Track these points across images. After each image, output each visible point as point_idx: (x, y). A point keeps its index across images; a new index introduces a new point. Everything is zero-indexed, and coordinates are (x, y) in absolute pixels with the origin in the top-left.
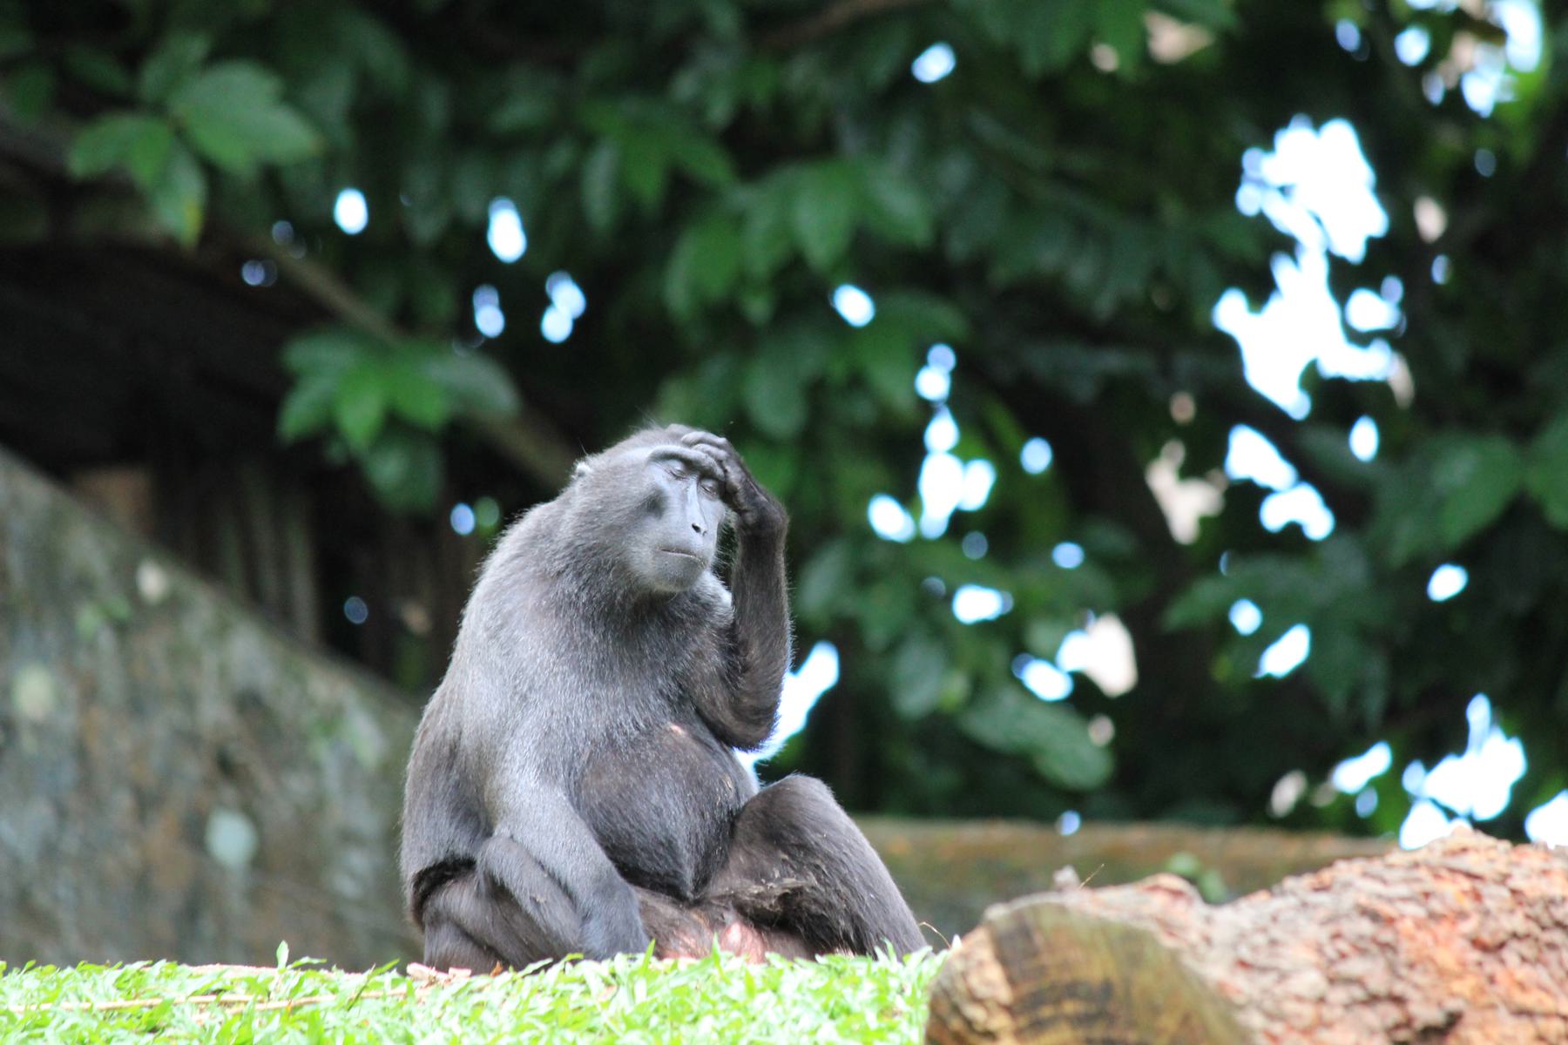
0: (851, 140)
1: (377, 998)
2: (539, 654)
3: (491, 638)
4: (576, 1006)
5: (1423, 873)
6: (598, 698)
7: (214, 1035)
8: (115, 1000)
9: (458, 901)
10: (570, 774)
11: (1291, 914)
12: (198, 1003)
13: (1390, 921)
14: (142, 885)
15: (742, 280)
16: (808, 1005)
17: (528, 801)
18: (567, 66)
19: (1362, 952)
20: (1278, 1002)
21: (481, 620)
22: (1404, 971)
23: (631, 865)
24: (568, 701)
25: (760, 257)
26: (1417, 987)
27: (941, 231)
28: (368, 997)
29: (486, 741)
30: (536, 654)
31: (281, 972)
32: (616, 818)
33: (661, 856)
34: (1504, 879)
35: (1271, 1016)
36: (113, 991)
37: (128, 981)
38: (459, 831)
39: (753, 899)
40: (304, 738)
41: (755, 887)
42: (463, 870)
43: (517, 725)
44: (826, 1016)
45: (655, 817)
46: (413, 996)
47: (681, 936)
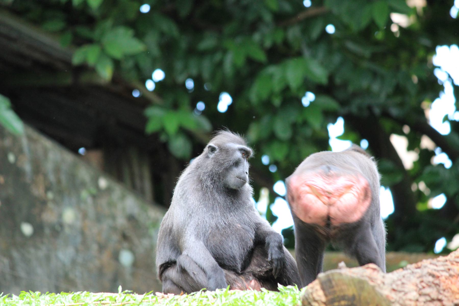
0: (307, 53)
1: (147, 302)
2: (194, 202)
3: (181, 198)
4: (205, 304)
5: (448, 263)
6: (212, 215)
8: (71, 303)
9: (172, 273)
10: (204, 237)
11: (409, 275)
12: (95, 304)
13: (438, 277)
14: (101, 271)
15: (272, 94)
16: (272, 303)
17: (192, 245)
18: (220, 32)
19: (429, 286)
21: (178, 193)
22: (442, 292)
23: (222, 263)
24: (204, 216)
25: (277, 87)
26: (446, 296)
27: (331, 78)
28: (144, 302)
29: (180, 228)
30: (194, 202)
31: (119, 295)
32: (219, 249)
33: (231, 261)
36: (71, 301)
37: (75, 298)
38: (172, 253)
39: (258, 272)
40: (147, 229)
41: (258, 269)
42: (173, 264)
43: (189, 223)
45: (230, 249)
47: (237, 283)
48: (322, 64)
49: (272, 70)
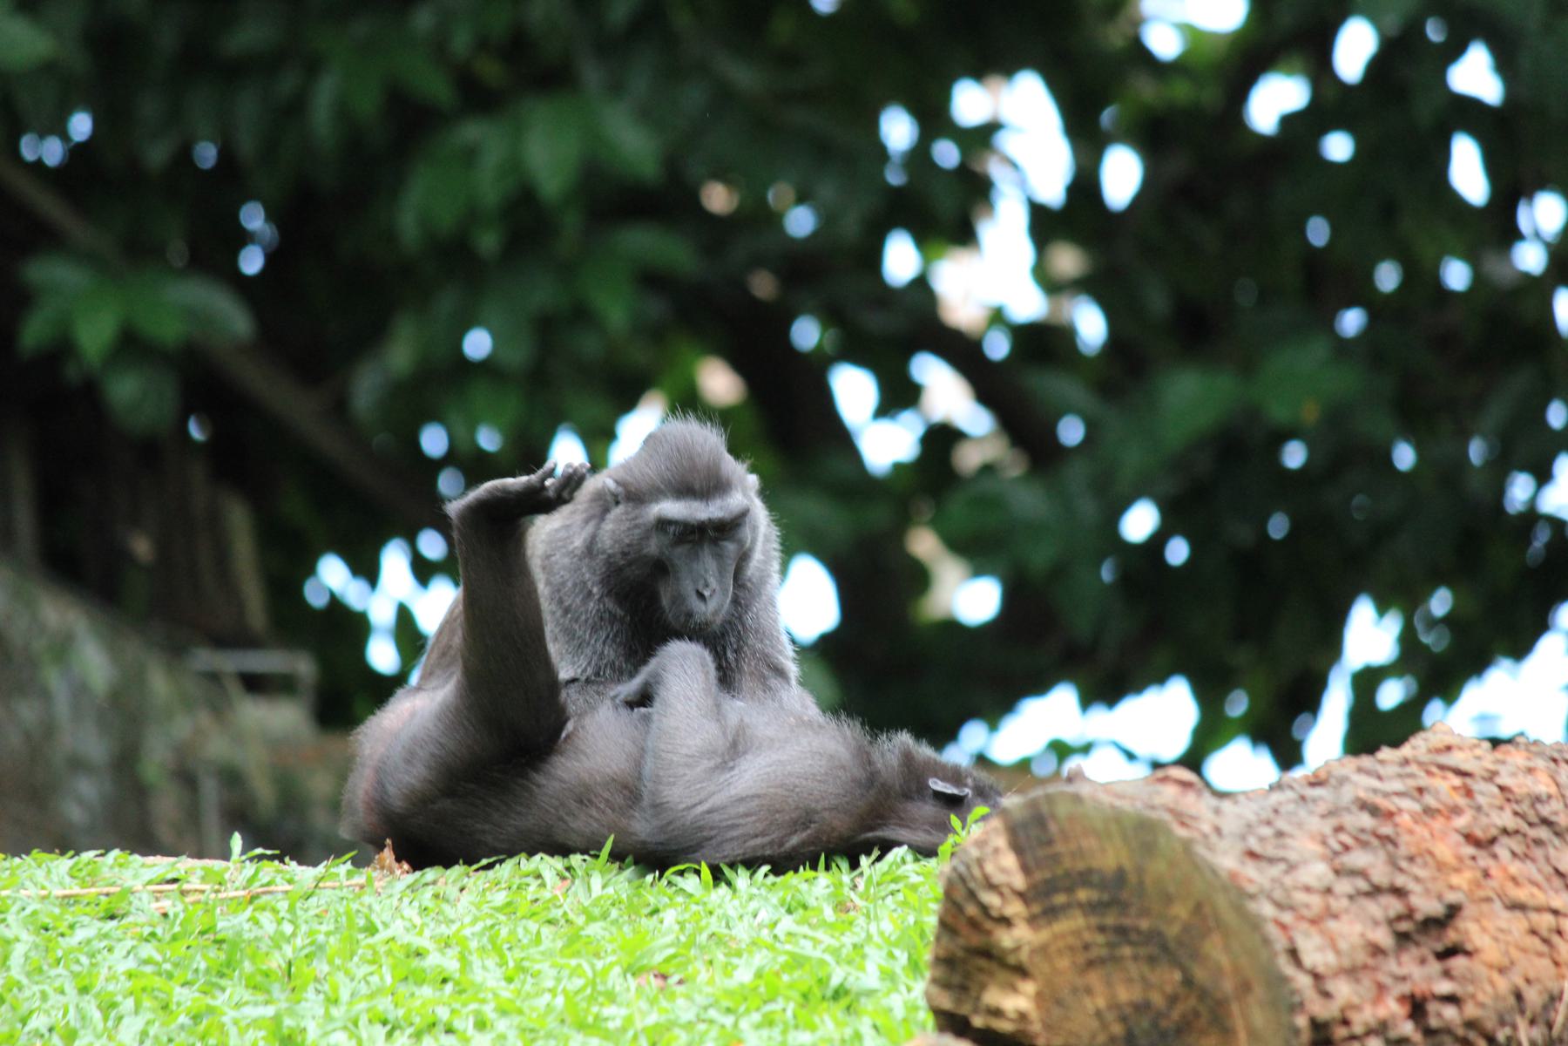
0: (591, 74)
1: (334, 888)
4: (534, 898)
5: (1413, 768)
7: (178, 922)
11: (1291, 807)
12: (154, 892)
13: (1390, 815)
15: (472, 216)
16: (766, 899)
19: (1364, 845)
20: (1287, 891)
22: (1404, 864)
25: (489, 187)
26: (1417, 879)
28: (325, 888)
34: (1491, 776)
35: (1279, 906)
36: (67, 879)
37: (80, 870)
44: (783, 911)
46: (373, 886)
48: (646, 115)
49: (472, 131)
